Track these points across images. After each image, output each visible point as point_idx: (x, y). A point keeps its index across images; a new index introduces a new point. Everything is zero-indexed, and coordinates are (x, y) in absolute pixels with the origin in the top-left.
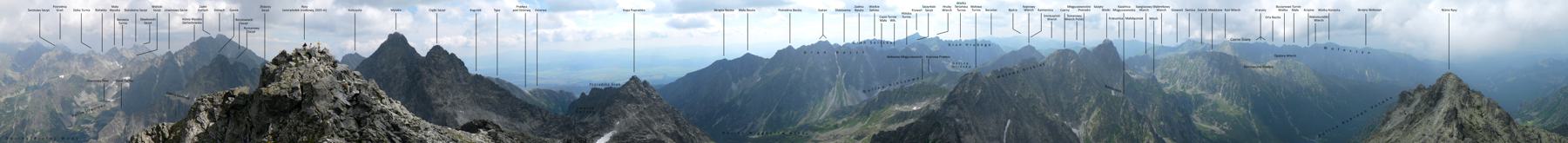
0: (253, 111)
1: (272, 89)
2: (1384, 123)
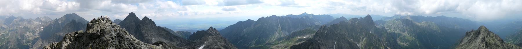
0: (84, 38)
1: (91, 31)
2: (461, 43)
